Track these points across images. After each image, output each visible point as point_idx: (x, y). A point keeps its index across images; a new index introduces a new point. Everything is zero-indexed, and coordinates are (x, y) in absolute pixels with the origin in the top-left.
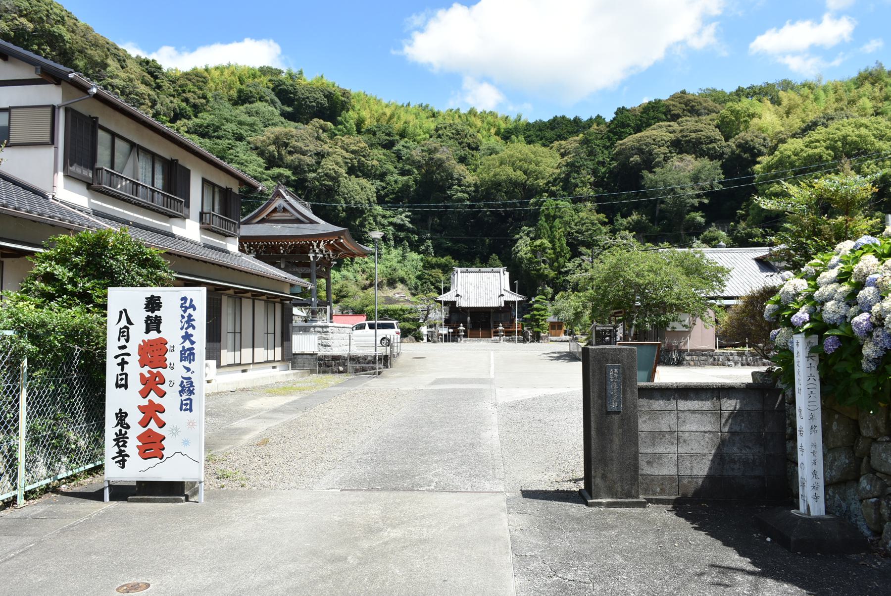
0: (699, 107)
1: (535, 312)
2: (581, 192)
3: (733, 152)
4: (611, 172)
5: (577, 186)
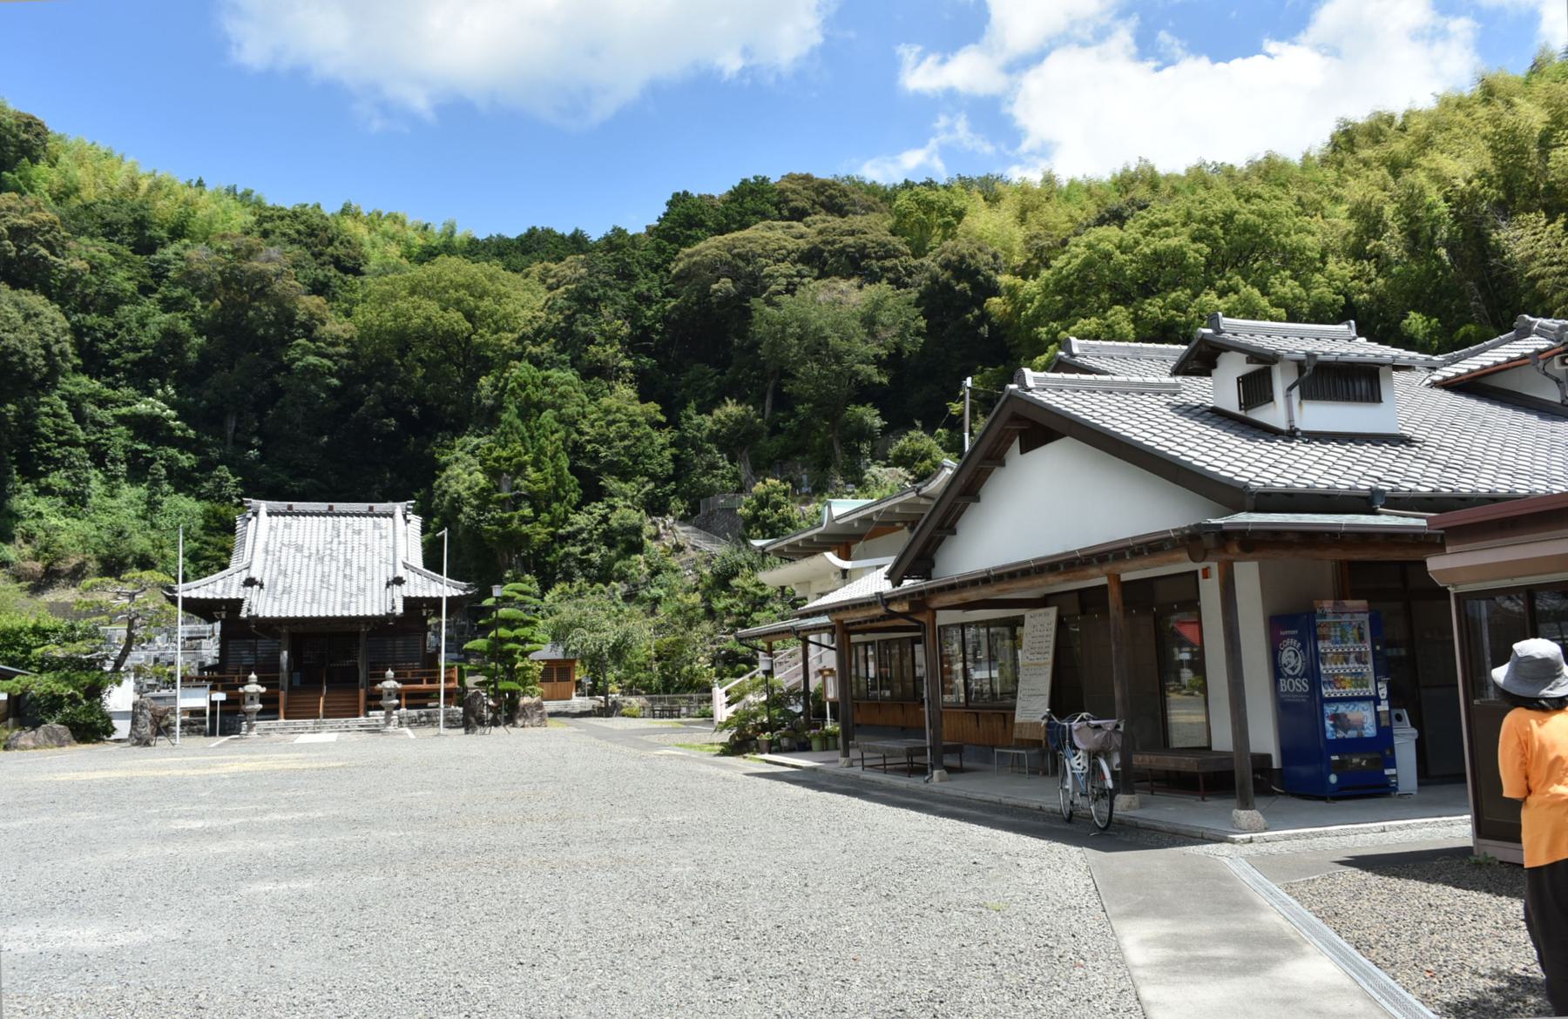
0: (843, 200)
1: (503, 632)
2: (602, 356)
3: (934, 279)
4: (665, 319)
5: (592, 341)
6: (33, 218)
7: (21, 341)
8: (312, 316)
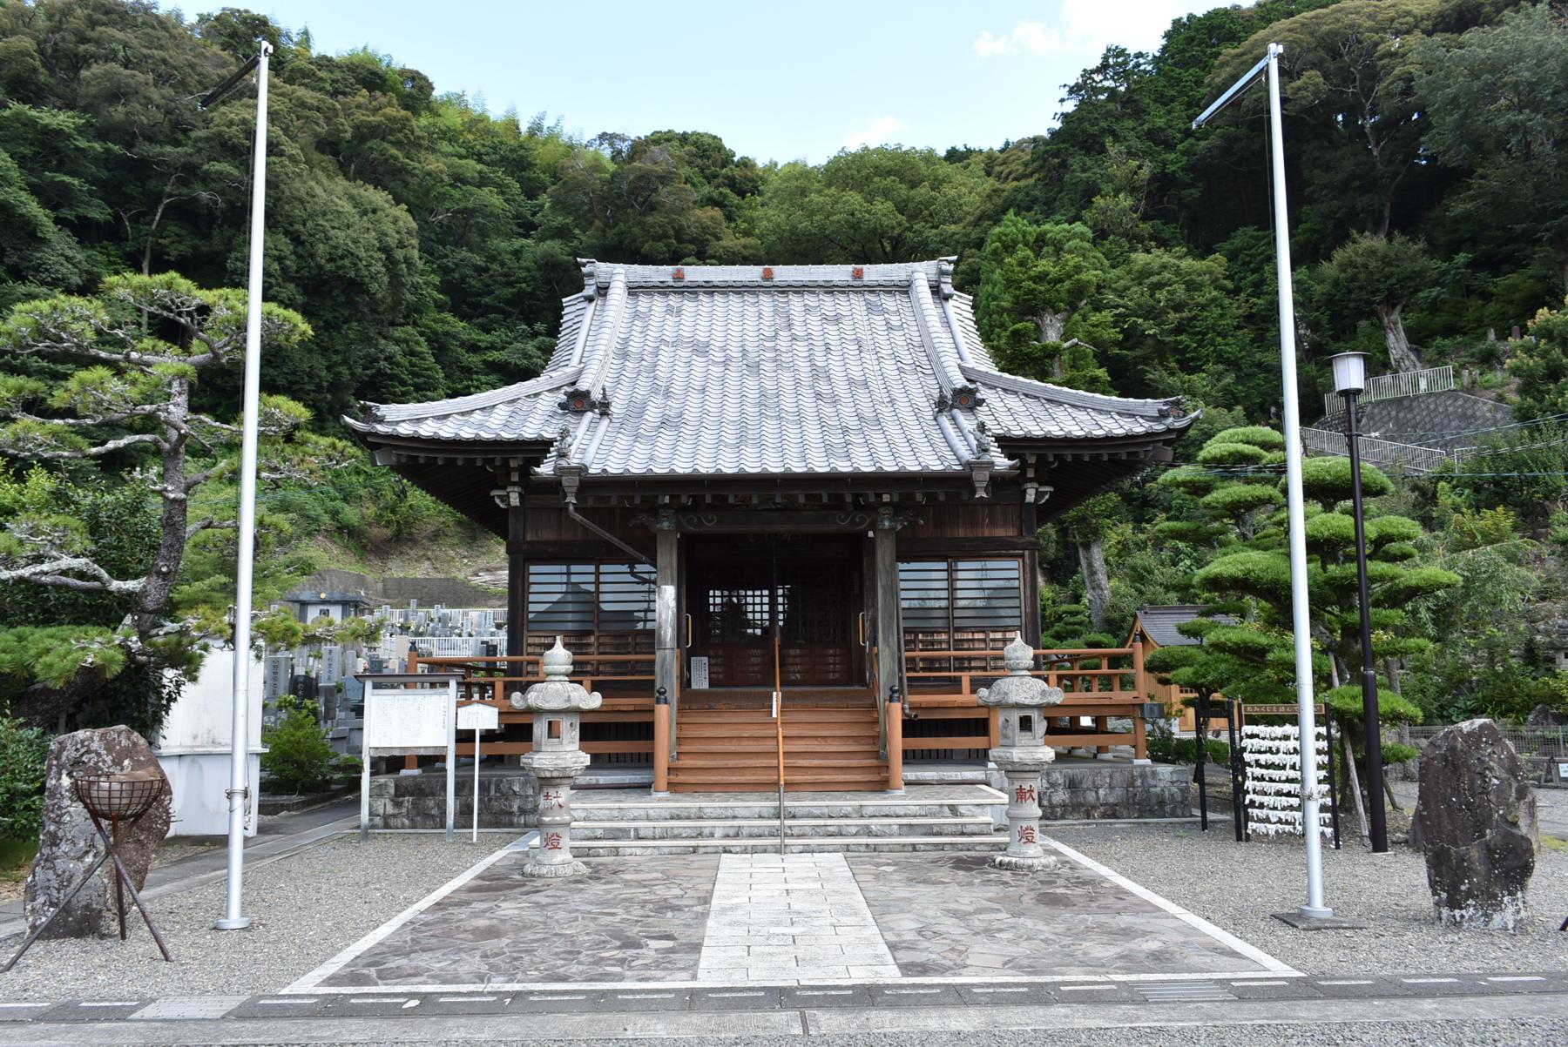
6: (384, 115)
7: (355, 242)
8: (705, 229)
